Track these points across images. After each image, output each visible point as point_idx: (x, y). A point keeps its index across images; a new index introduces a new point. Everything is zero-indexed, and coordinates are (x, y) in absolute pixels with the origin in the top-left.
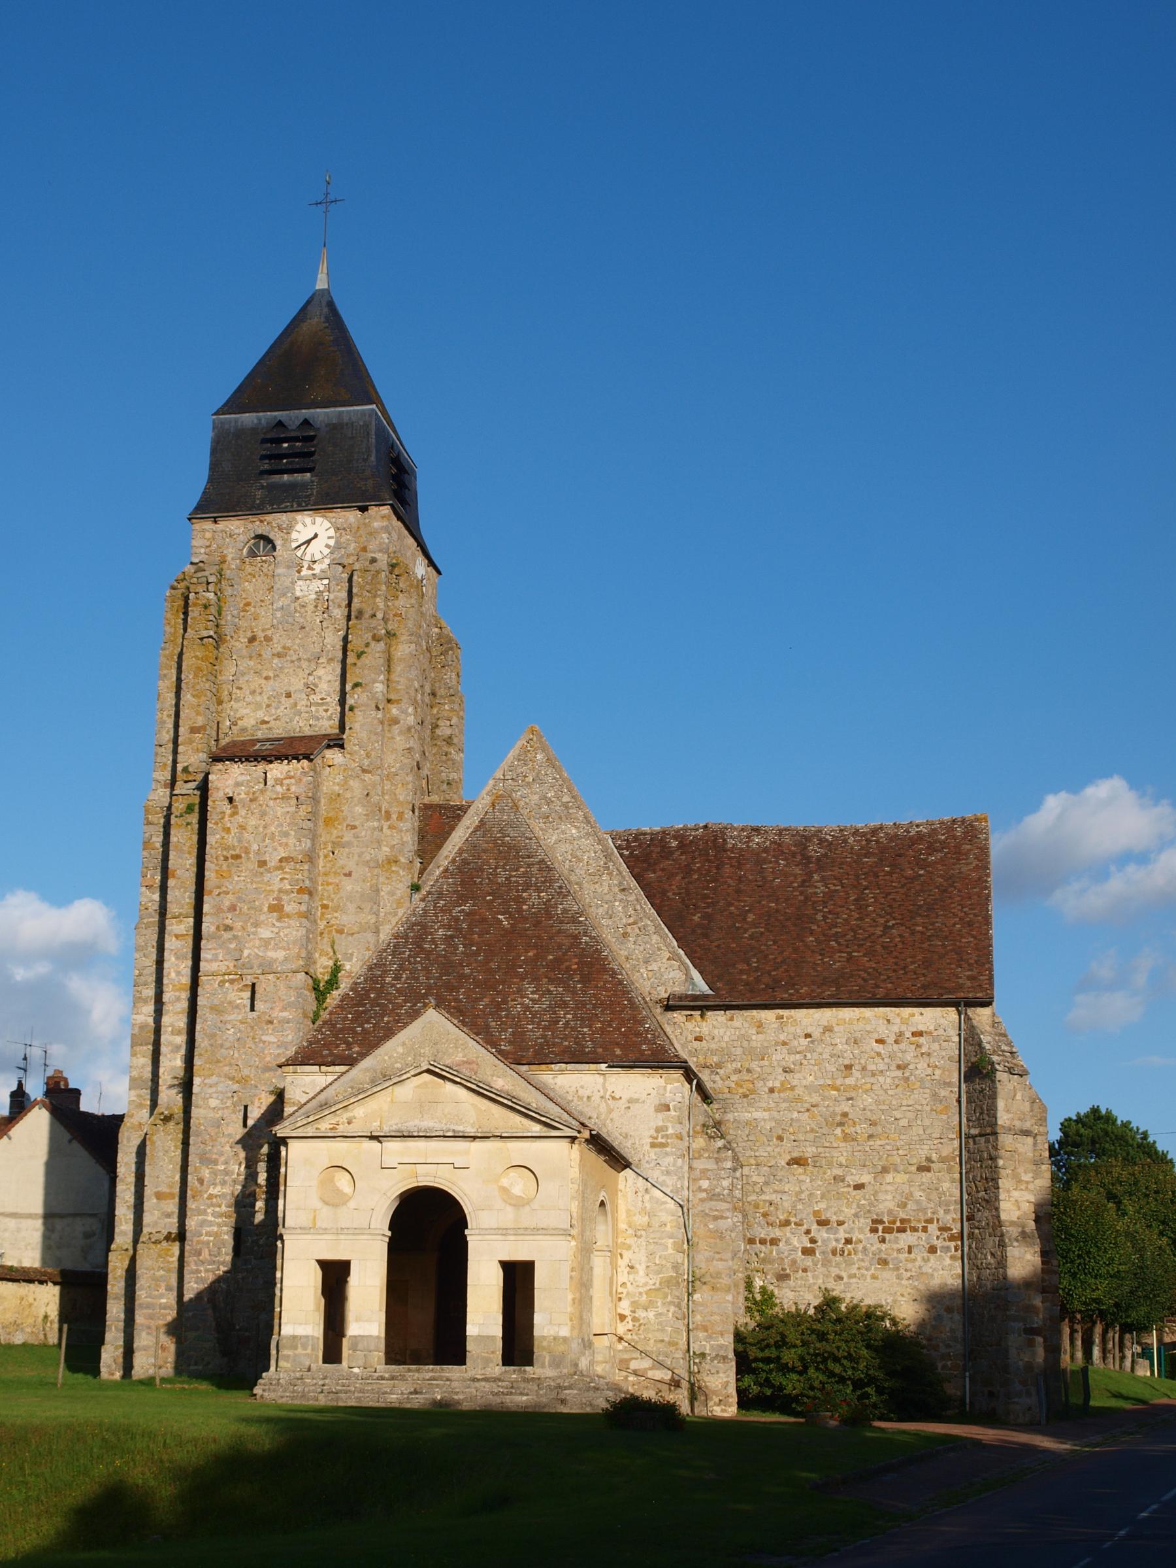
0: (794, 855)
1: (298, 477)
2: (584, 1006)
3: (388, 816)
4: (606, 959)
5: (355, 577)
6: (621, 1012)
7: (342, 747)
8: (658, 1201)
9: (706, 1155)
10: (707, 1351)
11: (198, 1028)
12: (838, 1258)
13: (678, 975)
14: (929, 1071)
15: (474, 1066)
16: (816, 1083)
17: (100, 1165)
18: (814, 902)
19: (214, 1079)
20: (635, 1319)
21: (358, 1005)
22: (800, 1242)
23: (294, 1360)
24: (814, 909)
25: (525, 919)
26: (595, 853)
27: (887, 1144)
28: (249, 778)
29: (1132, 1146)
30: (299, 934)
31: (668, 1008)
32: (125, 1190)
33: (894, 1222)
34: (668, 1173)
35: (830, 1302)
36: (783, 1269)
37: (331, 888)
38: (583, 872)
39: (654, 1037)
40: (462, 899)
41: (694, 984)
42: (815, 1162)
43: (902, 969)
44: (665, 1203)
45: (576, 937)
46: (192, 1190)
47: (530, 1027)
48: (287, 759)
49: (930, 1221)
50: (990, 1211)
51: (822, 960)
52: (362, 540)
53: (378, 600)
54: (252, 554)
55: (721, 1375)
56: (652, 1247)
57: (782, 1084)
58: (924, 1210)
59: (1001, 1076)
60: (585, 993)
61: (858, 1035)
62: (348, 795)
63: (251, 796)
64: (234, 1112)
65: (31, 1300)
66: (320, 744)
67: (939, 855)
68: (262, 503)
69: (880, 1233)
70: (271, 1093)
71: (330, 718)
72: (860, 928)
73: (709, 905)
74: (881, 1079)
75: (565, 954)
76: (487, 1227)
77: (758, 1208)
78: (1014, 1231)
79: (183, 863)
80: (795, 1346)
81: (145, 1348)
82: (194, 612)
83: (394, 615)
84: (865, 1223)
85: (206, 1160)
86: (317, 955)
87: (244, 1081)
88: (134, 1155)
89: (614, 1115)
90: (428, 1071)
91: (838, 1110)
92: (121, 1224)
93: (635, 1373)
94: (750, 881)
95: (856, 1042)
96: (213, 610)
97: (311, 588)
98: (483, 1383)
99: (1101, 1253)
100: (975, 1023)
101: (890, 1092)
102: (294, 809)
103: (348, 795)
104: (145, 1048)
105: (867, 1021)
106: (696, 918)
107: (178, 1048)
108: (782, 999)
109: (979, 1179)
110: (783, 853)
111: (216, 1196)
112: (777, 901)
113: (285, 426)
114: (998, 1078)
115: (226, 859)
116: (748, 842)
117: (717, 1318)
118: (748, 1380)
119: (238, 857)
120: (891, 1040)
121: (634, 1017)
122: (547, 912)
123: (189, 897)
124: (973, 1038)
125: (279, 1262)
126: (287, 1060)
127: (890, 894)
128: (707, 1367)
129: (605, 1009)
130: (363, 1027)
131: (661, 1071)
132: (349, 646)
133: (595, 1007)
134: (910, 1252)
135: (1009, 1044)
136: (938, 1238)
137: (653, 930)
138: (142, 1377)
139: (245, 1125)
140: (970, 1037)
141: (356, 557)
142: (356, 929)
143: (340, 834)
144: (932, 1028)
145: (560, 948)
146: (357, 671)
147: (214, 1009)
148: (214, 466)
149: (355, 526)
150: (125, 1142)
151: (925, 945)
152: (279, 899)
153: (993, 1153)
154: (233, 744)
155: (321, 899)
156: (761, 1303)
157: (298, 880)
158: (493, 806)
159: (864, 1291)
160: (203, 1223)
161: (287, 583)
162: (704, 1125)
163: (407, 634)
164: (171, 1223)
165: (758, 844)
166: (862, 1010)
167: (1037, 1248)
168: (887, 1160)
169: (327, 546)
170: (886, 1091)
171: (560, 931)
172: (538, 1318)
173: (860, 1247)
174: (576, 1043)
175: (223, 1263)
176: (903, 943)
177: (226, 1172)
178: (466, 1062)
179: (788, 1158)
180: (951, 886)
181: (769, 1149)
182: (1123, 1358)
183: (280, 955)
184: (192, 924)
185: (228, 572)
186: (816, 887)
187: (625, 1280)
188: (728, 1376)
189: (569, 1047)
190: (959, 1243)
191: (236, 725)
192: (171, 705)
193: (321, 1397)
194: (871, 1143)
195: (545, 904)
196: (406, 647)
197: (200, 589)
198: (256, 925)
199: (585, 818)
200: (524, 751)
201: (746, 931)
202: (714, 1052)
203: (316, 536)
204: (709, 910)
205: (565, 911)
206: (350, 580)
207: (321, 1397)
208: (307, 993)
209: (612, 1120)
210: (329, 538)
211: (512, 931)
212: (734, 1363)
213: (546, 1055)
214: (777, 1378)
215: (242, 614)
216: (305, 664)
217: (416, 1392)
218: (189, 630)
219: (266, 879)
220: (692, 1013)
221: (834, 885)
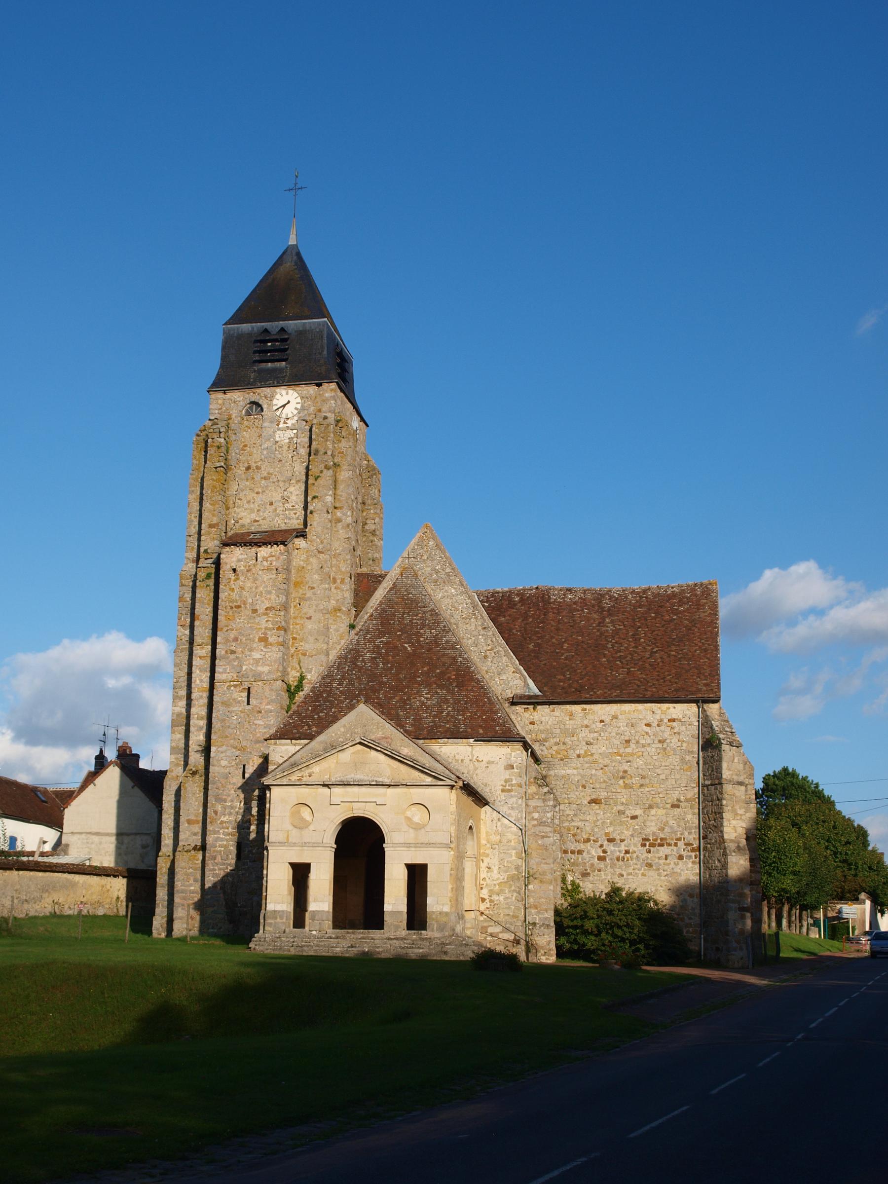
0: (593, 606)
1: (277, 364)
2: (459, 702)
4: (473, 672)
5: (314, 429)
8: (506, 826)
9: (537, 797)
10: (537, 922)
11: (214, 715)
12: (621, 863)
13: (520, 683)
14: (679, 744)
15: (390, 740)
16: (607, 751)
17: (152, 802)
18: (606, 636)
19: (224, 748)
20: (491, 901)
22: (596, 852)
23: (275, 926)
24: (606, 640)
25: (422, 647)
27: (652, 790)
28: (246, 556)
30: (278, 656)
31: (513, 704)
32: (168, 818)
33: (656, 840)
34: (512, 808)
37: (298, 626)
38: (458, 617)
40: (382, 634)
41: (529, 688)
43: (662, 679)
44: (511, 827)
45: (454, 658)
46: (210, 818)
47: (425, 715)
48: (270, 544)
49: (679, 839)
50: (718, 833)
51: (611, 673)
52: (318, 405)
53: (328, 443)
54: (248, 414)
57: (585, 752)
58: (675, 832)
59: (725, 747)
61: (634, 721)
62: (309, 568)
63: (247, 568)
64: (237, 769)
65: (108, 887)
67: (687, 606)
68: (255, 381)
69: (647, 847)
70: (260, 757)
71: (298, 518)
72: (636, 653)
73: (539, 638)
74: (649, 749)
75: (447, 669)
77: (570, 831)
78: (732, 846)
79: (204, 611)
81: (181, 918)
82: (211, 451)
83: (339, 453)
84: (638, 840)
85: (219, 799)
87: (243, 749)
88: (173, 796)
89: (478, 771)
90: (360, 743)
91: (621, 769)
92: (166, 840)
93: (491, 935)
94: (566, 623)
95: (632, 726)
96: (223, 449)
97: (286, 435)
98: (395, 941)
100: (708, 713)
101: (654, 757)
102: (275, 576)
103: (309, 568)
104: (180, 728)
105: (639, 712)
106: (531, 646)
107: (201, 728)
108: (586, 698)
109: (710, 813)
110: (586, 605)
111: (225, 822)
112: (583, 635)
114: (723, 749)
115: (232, 608)
117: (543, 900)
118: (563, 940)
119: (239, 607)
120: (655, 724)
121: (491, 710)
122: (436, 642)
123: (208, 632)
124: (707, 723)
125: (265, 864)
126: (270, 736)
127: (654, 631)
130: (318, 715)
131: (508, 744)
132: (310, 473)
133: (466, 703)
134: (666, 859)
135: (730, 727)
136: (684, 850)
139: (244, 777)
140: (705, 722)
143: (304, 592)
144: (681, 717)
145: (444, 665)
146: (315, 488)
148: (224, 358)
150: (168, 788)
151: (677, 664)
152: (265, 634)
153: (720, 796)
155: (292, 634)
157: (277, 622)
158: (402, 574)
160: (217, 839)
161: (271, 432)
162: (535, 778)
165: (570, 599)
166: (637, 705)
167: (747, 857)
168: (652, 801)
169: (296, 409)
170: (651, 757)
171: (444, 654)
172: (430, 900)
173: (635, 855)
174: (454, 726)
175: (230, 865)
176: (663, 662)
177: (232, 807)
178: (384, 738)
180: (694, 626)
181: (577, 793)
182: (801, 926)
183: (266, 669)
185: (233, 425)
186: (607, 627)
189: (450, 728)
190: (698, 853)
191: (238, 523)
192: (197, 510)
195: (434, 637)
196: (346, 473)
197: (215, 436)
198: (251, 650)
199: (460, 582)
200: (421, 540)
201: (563, 654)
202: (542, 732)
203: (289, 402)
204: (539, 641)
205: (447, 642)
206: (311, 430)
207: (292, 949)
208: (283, 693)
210: (297, 403)
211: (414, 654)
212: (554, 929)
214: (582, 939)
215: (242, 452)
216: (281, 484)
217: (352, 946)
218: (208, 462)
220: (528, 706)
221: (619, 625)
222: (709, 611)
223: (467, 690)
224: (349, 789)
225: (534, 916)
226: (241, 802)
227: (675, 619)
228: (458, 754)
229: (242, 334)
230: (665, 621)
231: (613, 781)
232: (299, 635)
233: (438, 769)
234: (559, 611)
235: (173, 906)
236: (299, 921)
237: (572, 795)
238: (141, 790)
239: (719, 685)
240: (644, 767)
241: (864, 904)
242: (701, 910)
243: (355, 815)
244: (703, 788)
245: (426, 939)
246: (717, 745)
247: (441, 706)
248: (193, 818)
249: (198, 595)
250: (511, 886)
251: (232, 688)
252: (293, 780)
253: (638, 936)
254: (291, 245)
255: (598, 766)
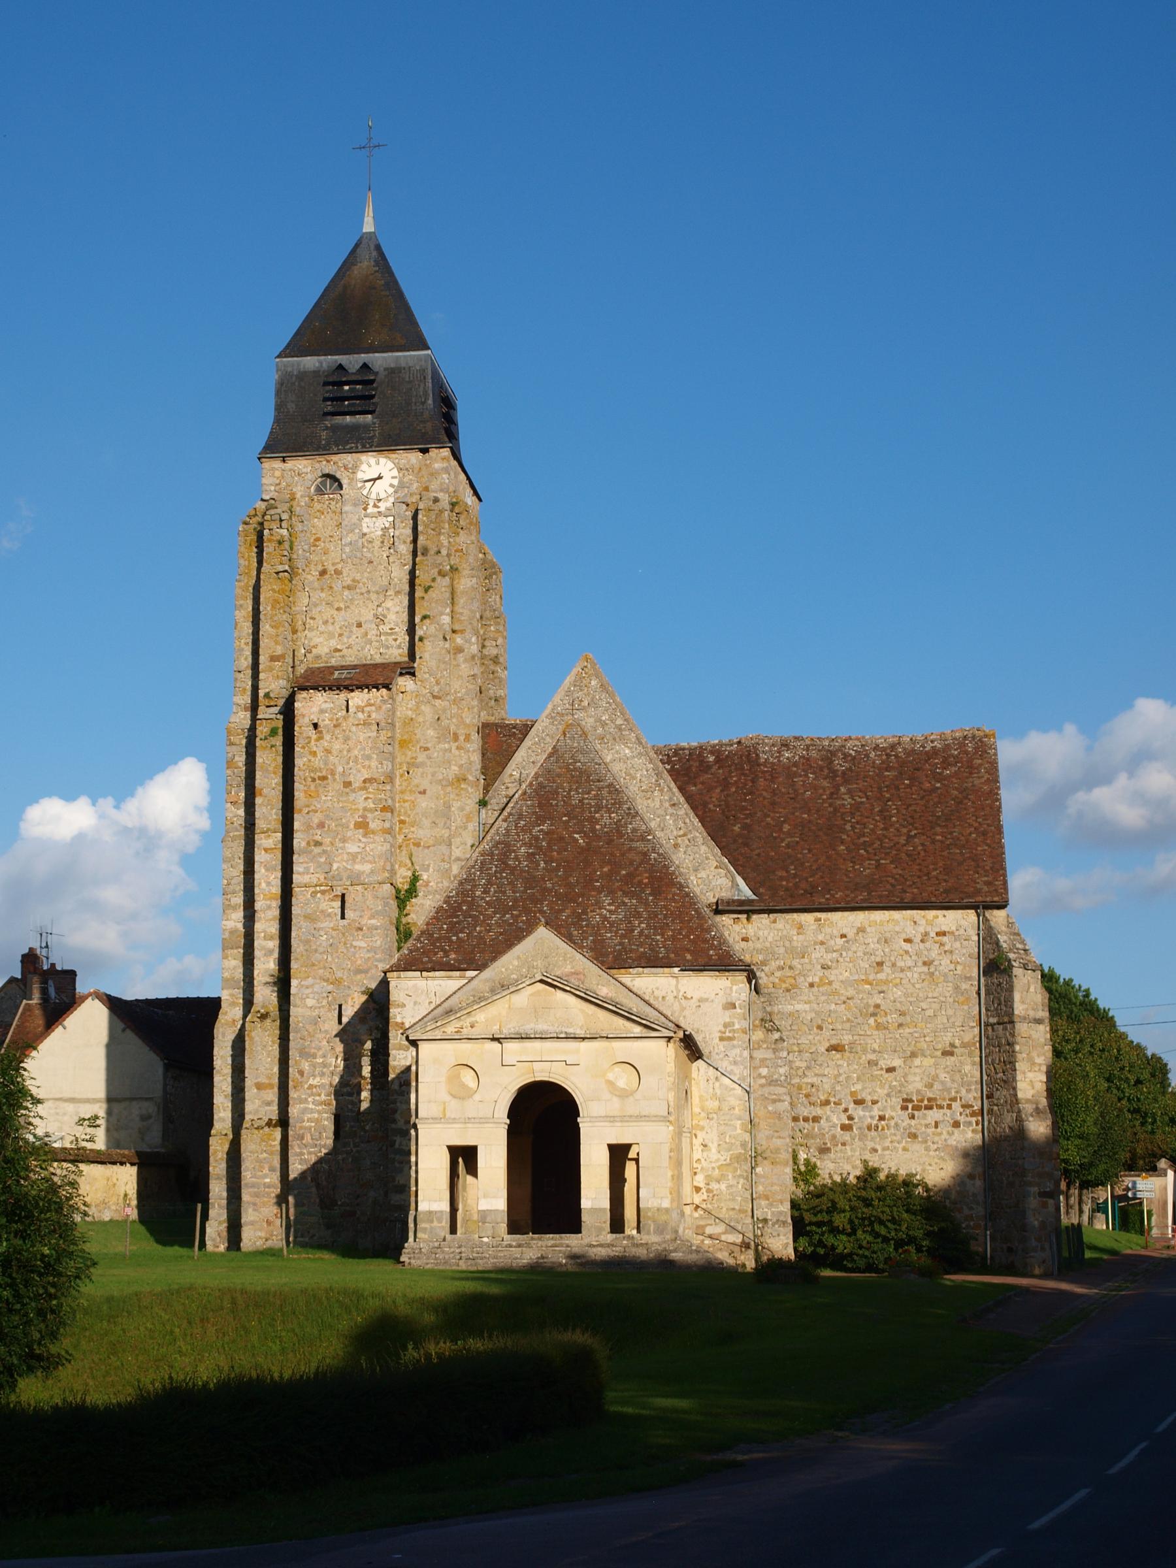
0: (821, 768)
1: (360, 419)
2: (656, 916)
3: (456, 737)
4: (673, 873)
5: (420, 516)
6: (690, 921)
7: (413, 674)
8: (727, 1087)
9: (765, 1046)
10: (769, 1217)
12: (873, 1133)
13: (725, 882)
14: (952, 967)
15: (582, 977)
16: (851, 978)
17: (155, 1052)
18: (843, 814)
19: (310, 981)
20: (708, 1191)
21: (451, 917)
22: (840, 1119)
24: (843, 819)
25: (599, 838)
26: (647, 771)
27: (916, 1032)
29: (1075, 1004)
30: (384, 849)
31: (718, 912)
32: (222, 1081)
33: (922, 1101)
34: (735, 1063)
35: (870, 1174)
36: (825, 1144)
37: (407, 804)
39: (720, 944)
40: (540, 820)
41: (739, 890)
42: (852, 1048)
44: (734, 1089)
45: (645, 854)
46: (293, 1081)
47: (609, 935)
48: (367, 688)
49: (954, 1099)
50: (1008, 1090)
52: (423, 480)
53: (442, 537)
54: (320, 491)
55: (781, 1237)
56: (722, 1128)
57: (821, 980)
58: (949, 1090)
59: (1017, 971)
60: (656, 905)
61: (888, 935)
62: (421, 719)
64: (329, 1010)
65: (115, 1181)
66: (395, 672)
67: (954, 769)
68: (328, 444)
69: (910, 1111)
70: (363, 993)
71: (399, 647)
74: (909, 974)
75: (636, 869)
76: (595, 1115)
77: (801, 1089)
79: (269, 782)
80: (844, 1211)
81: (252, 1223)
82: (268, 548)
83: (456, 551)
84: (897, 1101)
85: (304, 1054)
86: (397, 866)
87: (337, 982)
88: (229, 1049)
89: (686, 1013)
90: (541, 981)
91: (871, 1002)
93: (710, 1237)
96: (287, 545)
97: (377, 524)
98: (600, 1249)
99: (1073, 1117)
100: (992, 924)
102: (375, 734)
103: (421, 719)
104: (235, 951)
105: (897, 922)
106: (737, 828)
107: (271, 952)
108: (820, 903)
109: (997, 1062)
110: (811, 767)
111: (316, 1087)
112: (809, 812)
113: (344, 369)
115: (314, 780)
116: (779, 757)
118: (803, 1241)
119: (324, 778)
120: (917, 939)
121: (701, 926)
122: (618, 831)
123: (276, 814)
124: (991, 938)
125: (413, 1148)
126: (391, 967)
127: (910, 805)
128: (769, 1231)
129: (675, 919)
131: (727, 974)
132: (417, 581)
133: (666, 917)
134: (936, 1127)
135: (1023, 942)
136: (961, 1114)
137: (702, 841)
138: (250, 1249)
139: (340, 1022)
140: (988, 936)
141: (418, 497)
142: (431, 842)
144: (954, 928)
145: (631, 863)
147: (307, 917)
148: (279, 408)
149: (417, 467)
150: (220, 1037)
151: (945, 853)
152: (364, 817)
153: (1010, 1039)
154: (311, 672)
155: (399, 815)
156: (806, 1173)
159: (896, 1161)
160: (305, 1110)
163: (469, 568)
164: (272, 1111)
166: (892, 912)
167: (1049, 1122)
168: (915, 1046)
169: (392, 485)
171: (630, 849)
173: (892, 1123)
174: (650, 949)
175: (324, 1146)
176: (925, 851)
177: (324, 1065)
179: (827, 1045)
180: (966, 798)
181: (810, 1037)
182: (1081, 1211)
183: (367, 867)
184: (280, 838)
185: (298, 509)
186: (843, 799)
187: (700, 1157)
188: (788, 1238)
190: (980, 1118)
191: (310, 652)
192: (248, 634)
193: (461, 1263)
194: (901, 1031)
195: (616, 824)
196: (468, 580)
197: (274, 526)
198: (344, 840)
199: (638, 739)
200: (580, 677)
201: (783, 840)
202: (759, 951)
203: (380, 478)
204: (748, 821)
205: (634, 830)
206: (415, 518)
208: (392, 902)
209: (684, 1017)
210: (393, 478)
211: (587, 849)
212: (791, 1227)
213: (625, 961)
214: (830, 1240)
215: (312, 548)
216: (373, 596)
218: (265, 564)
219: (351, 798)
220: (739, 916)
221: (860, 797)
222: (987, 776)
223: (666, 898)
224: (528, 1044)
225: (764, 1210)
226: (337, 1058)
227: (938, 788)
228: (657, 989)
229: (305, 372)
230: (925, 791)
231: (860, 1020)
232: (409, 816)
233: (650, 1015)
234: (773, 777)
235: (239, 1206)
236: (617, 1225)
237: (803, 1040)
238: (137, 1034)
239: (1005, 883)
240: (903, 999)
241: (1166, 1176)
242: (985, 1197)
243: (537, 1079)
244: (986, 1028)
245: (642, 1244)
246: (1005, 969)
247: (630, 922)
248: (263, 1080)
249: (259, 760)
250: (735, 1170)
251: (319, 895)
252: (449, 1032)
253: (907, 1235)
254: (366, 233)
255: (839, 999)
